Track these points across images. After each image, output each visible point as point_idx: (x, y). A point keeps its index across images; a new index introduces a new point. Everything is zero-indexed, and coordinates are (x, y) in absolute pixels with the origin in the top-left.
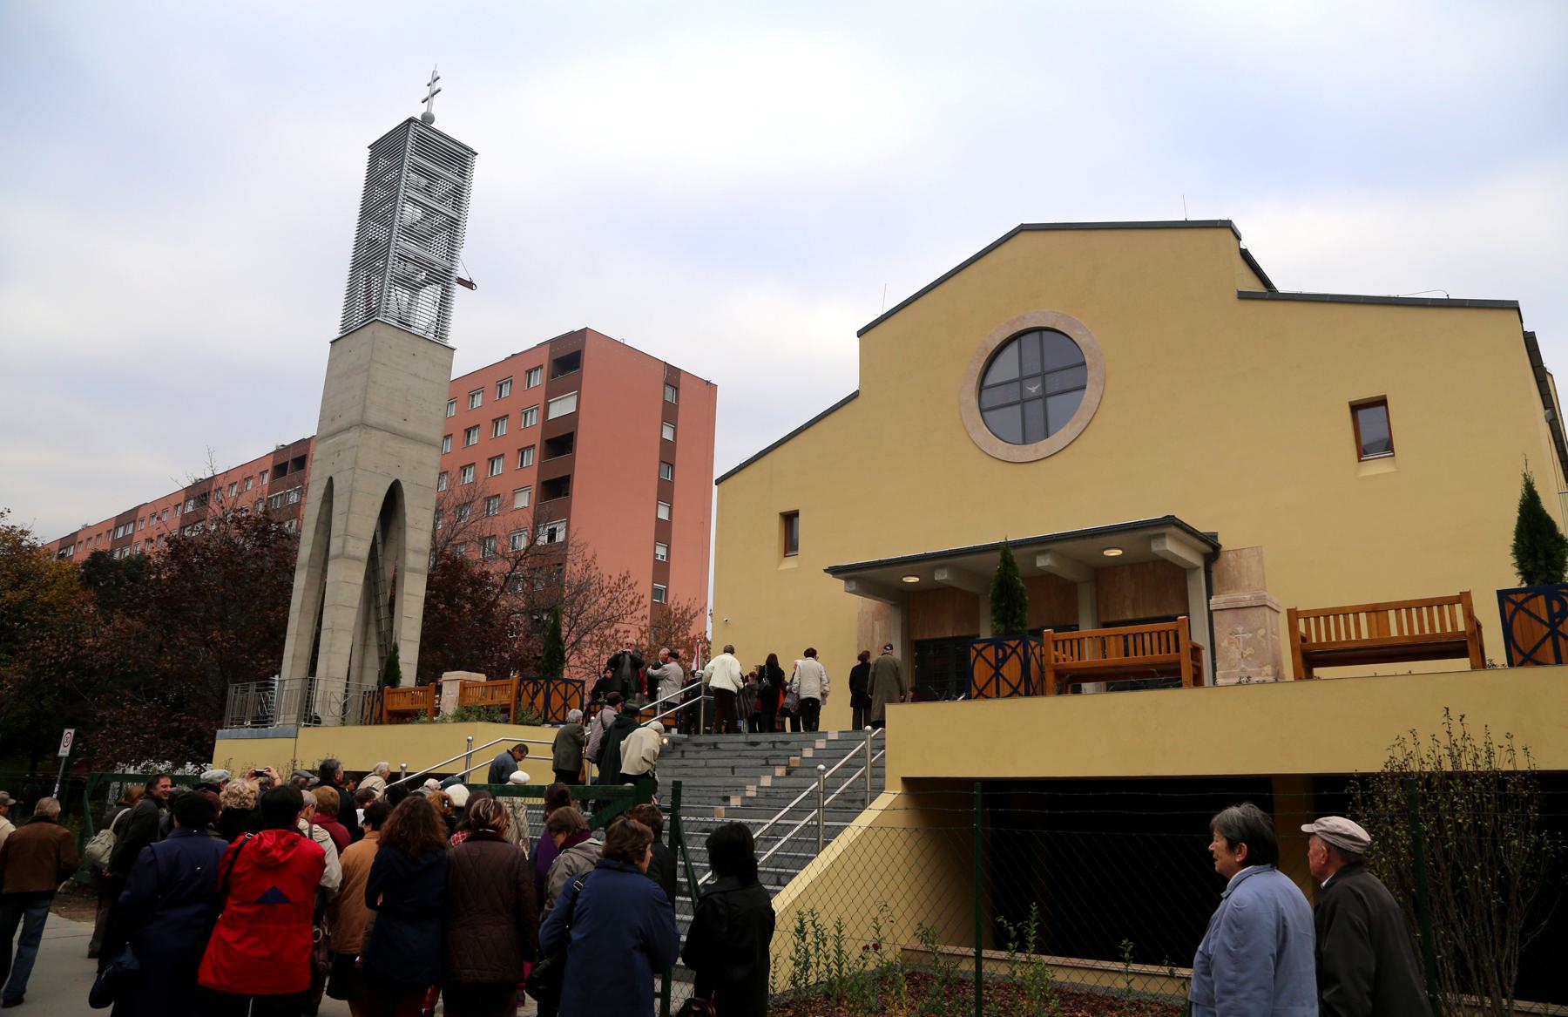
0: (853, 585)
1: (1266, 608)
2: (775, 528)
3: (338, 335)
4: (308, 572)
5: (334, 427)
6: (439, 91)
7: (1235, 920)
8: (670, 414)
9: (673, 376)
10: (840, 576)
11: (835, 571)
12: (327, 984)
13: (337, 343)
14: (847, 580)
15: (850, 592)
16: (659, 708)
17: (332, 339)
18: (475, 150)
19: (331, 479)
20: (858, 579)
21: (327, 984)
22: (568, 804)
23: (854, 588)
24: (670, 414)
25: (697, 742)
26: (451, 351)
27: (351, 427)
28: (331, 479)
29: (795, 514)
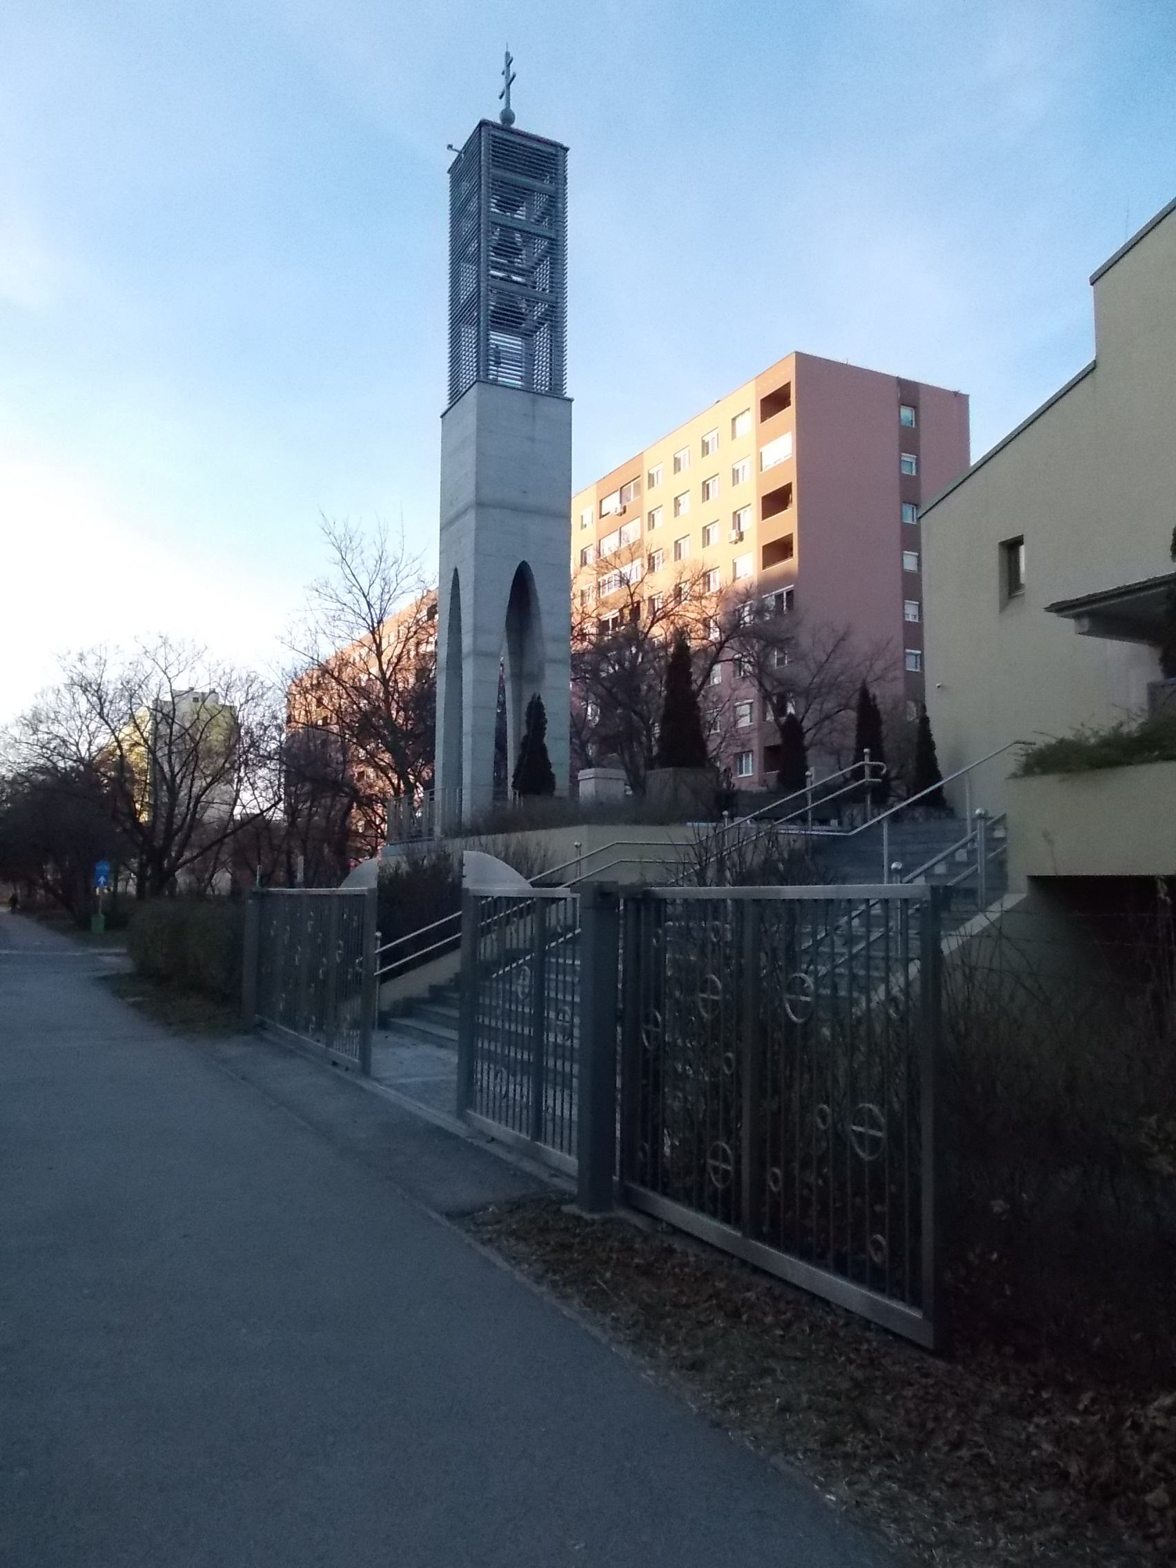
0: (1086, 622)
1: (738, 420)
2: (992, 559)
3: (447, 407)
4: (447, 674)
5: (452, 512)
6: (514, 77)
7: (549, 855)
8: (909, 440)
9: (909, 392)
10: (1066, 613)
11: (1060, 608)
12: (618, 1126)
13: (447, 416)
14: (1077, 617)
15: (1083, 634)
16: (810, 796)
17: (441, 414)
18: (565, 145)
19: (456, 570)
20: (1091, 615)
21: (618, 1126)
22: (382, 856)
23: (1086, 629)
24: (909, 440)
25: (567, 784)
26: (568, 403)
27: (466, 510)
28: (456, 570)
29: (1018, 542)
